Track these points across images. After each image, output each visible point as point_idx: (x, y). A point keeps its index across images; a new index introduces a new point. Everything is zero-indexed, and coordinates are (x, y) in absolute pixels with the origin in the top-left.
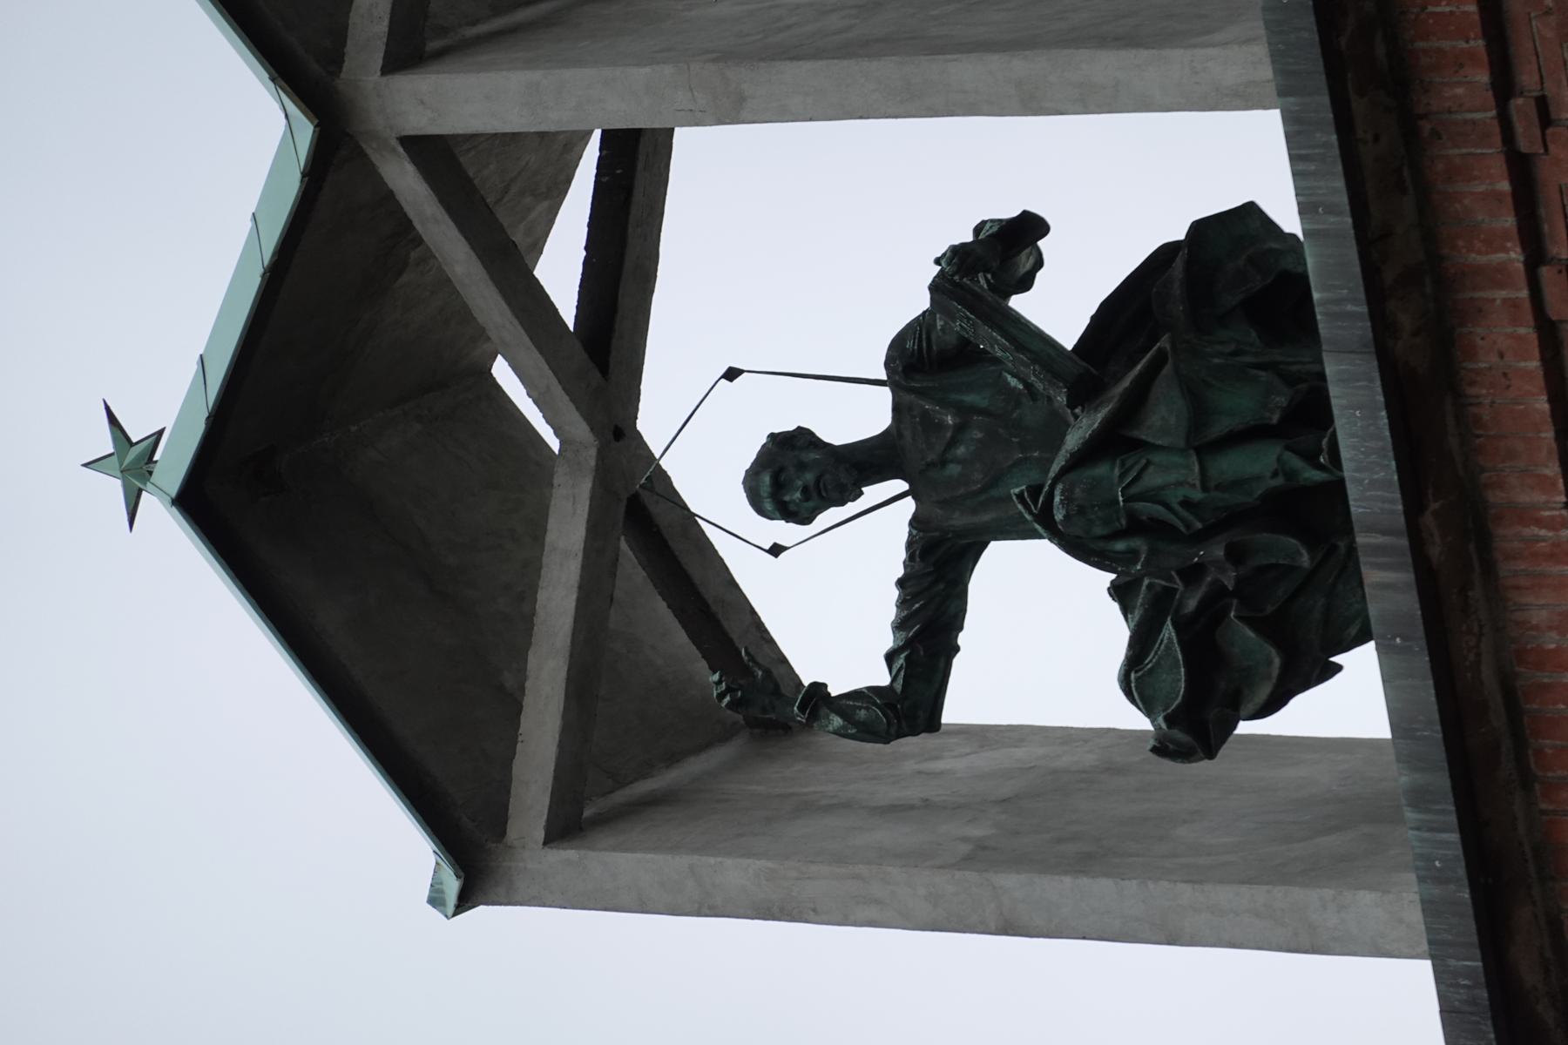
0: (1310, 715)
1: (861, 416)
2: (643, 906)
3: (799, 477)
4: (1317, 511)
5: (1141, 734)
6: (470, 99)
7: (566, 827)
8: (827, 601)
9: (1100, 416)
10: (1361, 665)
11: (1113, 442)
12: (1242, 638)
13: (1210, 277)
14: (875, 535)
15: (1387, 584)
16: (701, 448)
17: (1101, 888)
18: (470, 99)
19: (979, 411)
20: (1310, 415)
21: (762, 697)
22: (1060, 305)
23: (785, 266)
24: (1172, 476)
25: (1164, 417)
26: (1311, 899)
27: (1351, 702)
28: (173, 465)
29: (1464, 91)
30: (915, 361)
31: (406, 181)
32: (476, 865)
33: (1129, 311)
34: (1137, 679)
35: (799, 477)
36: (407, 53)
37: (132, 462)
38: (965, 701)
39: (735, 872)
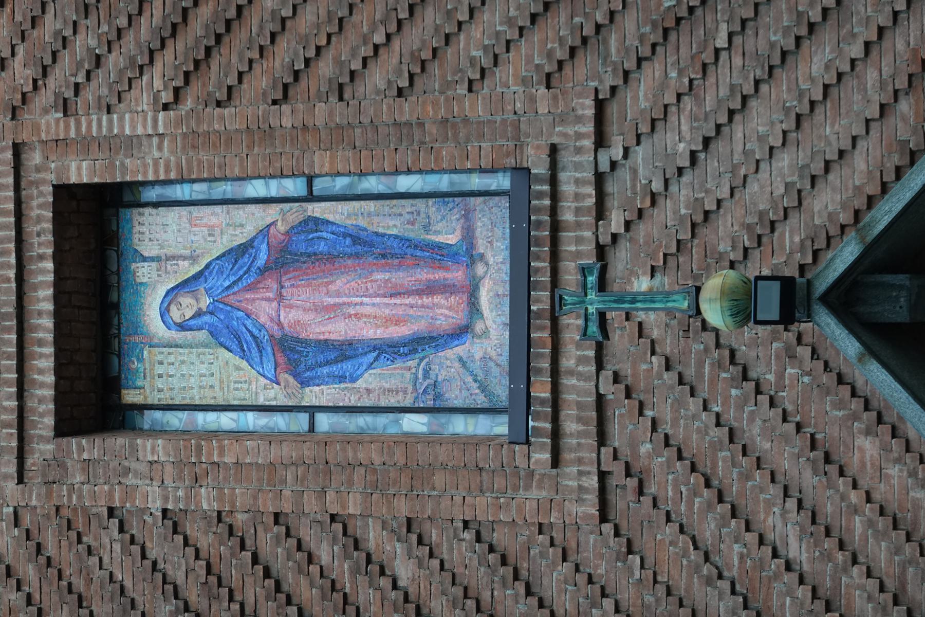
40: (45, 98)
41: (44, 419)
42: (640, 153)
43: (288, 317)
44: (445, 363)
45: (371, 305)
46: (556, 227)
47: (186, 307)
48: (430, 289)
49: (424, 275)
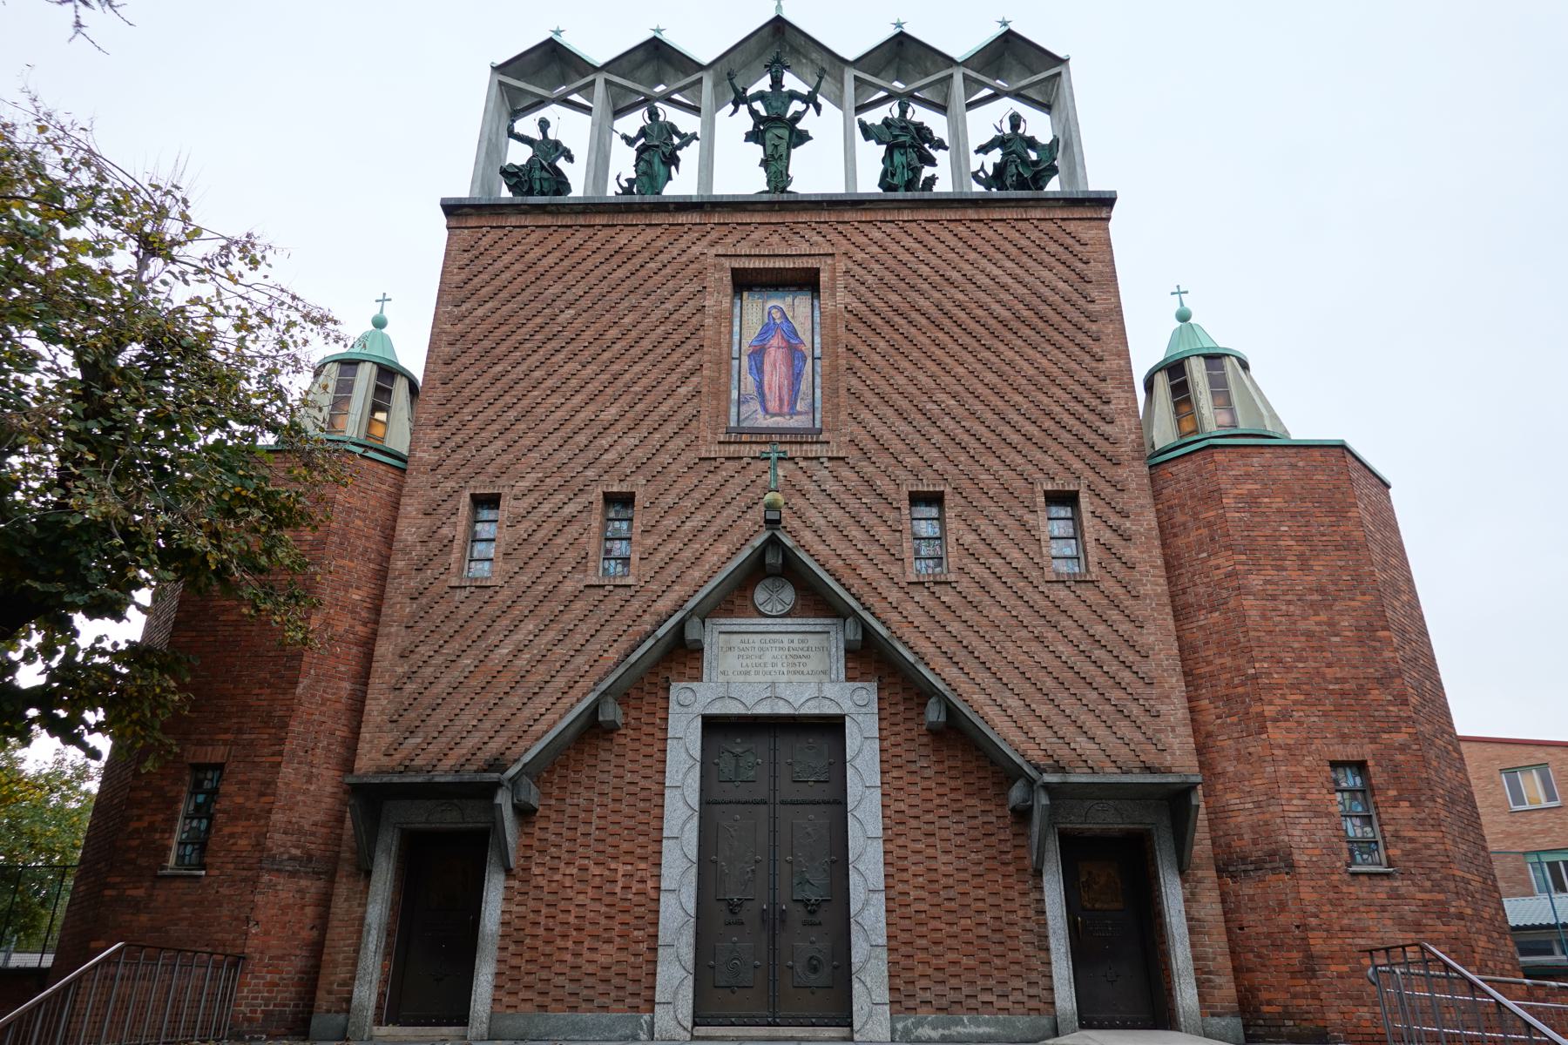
0: (505, 187)
1: (551, 135)
2: (1112, 1026)
3: (544, 125)
4: (530, 192)
5: (605, 190)
6: (600, 88)
7: (501, 83)
8: (527, 125)
9: (378, 907)
10: (510, 195)
11: (543, 168)
12: (515, 180)
13: (562, 185)
14: (538, 136)
15: (519, 200)
16: (552, 112)
17: (483, 155)
18: (600, 88)
19: (549, 150)
20: (543, 194)
21: (516, 114)
22: (561, 163)
23: (570, 127)
24: (537, 174)
25: (545, 175)
26: (478, 184)
27: (506, 193)
28: (556, 38)
29: (581, 220)
30: (557, 144)
31: (590, 78)
32: (498, 69)
33: (559, 172)
34: (511, 165)
35: (544, 125)
36: (607, 82)
37: (558, 32)
38: (512, 141)
39: (491, 105)
40: (851, 265)
41: (737, 264)
42: (826, 472)
43: (772, 351)
44: (755, 405)
45: (776, 379)
46: (801, 443)
47: (776, 315)
48: (781, 400)
49: (786, 398)
